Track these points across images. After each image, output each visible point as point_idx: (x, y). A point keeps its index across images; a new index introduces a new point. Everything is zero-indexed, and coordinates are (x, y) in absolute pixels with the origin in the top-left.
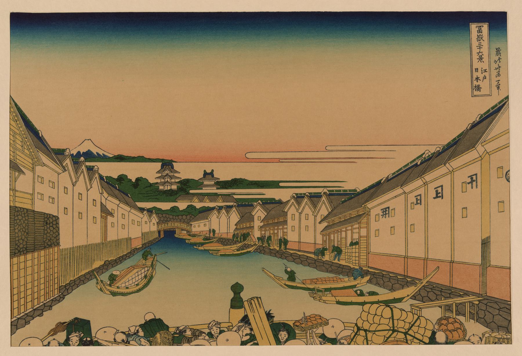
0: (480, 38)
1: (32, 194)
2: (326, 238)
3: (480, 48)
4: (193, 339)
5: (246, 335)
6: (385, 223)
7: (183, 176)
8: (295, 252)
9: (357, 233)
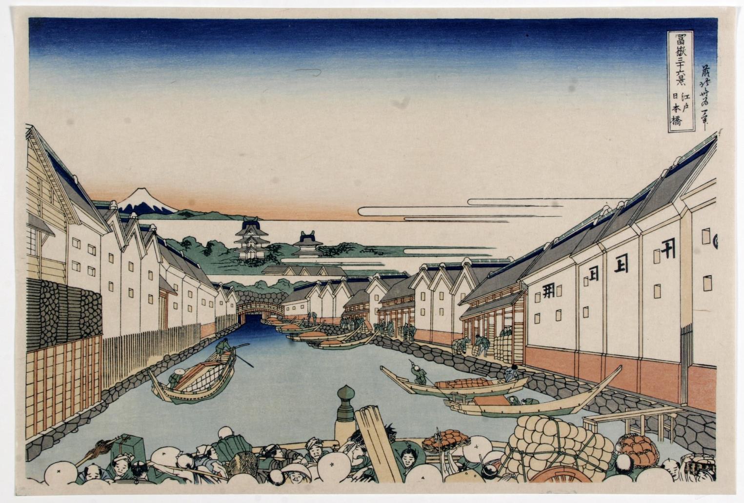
3: (680, 65)
6: (547, 306)
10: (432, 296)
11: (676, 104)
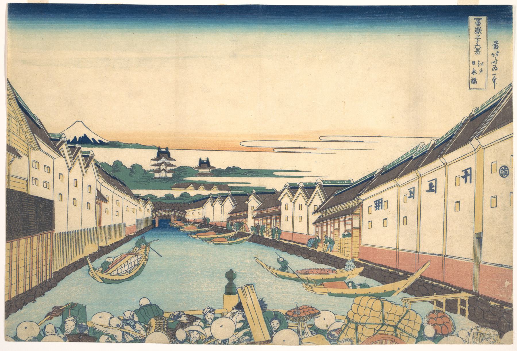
1: (27, 180)
2: (319, 230)
3: (478, 41)
4: (188, 325)
5: (240, 322)
6: (378, 215)
7: (178, 163)
8: (288, 242)
10: (294, 206)
11: (474, 69)
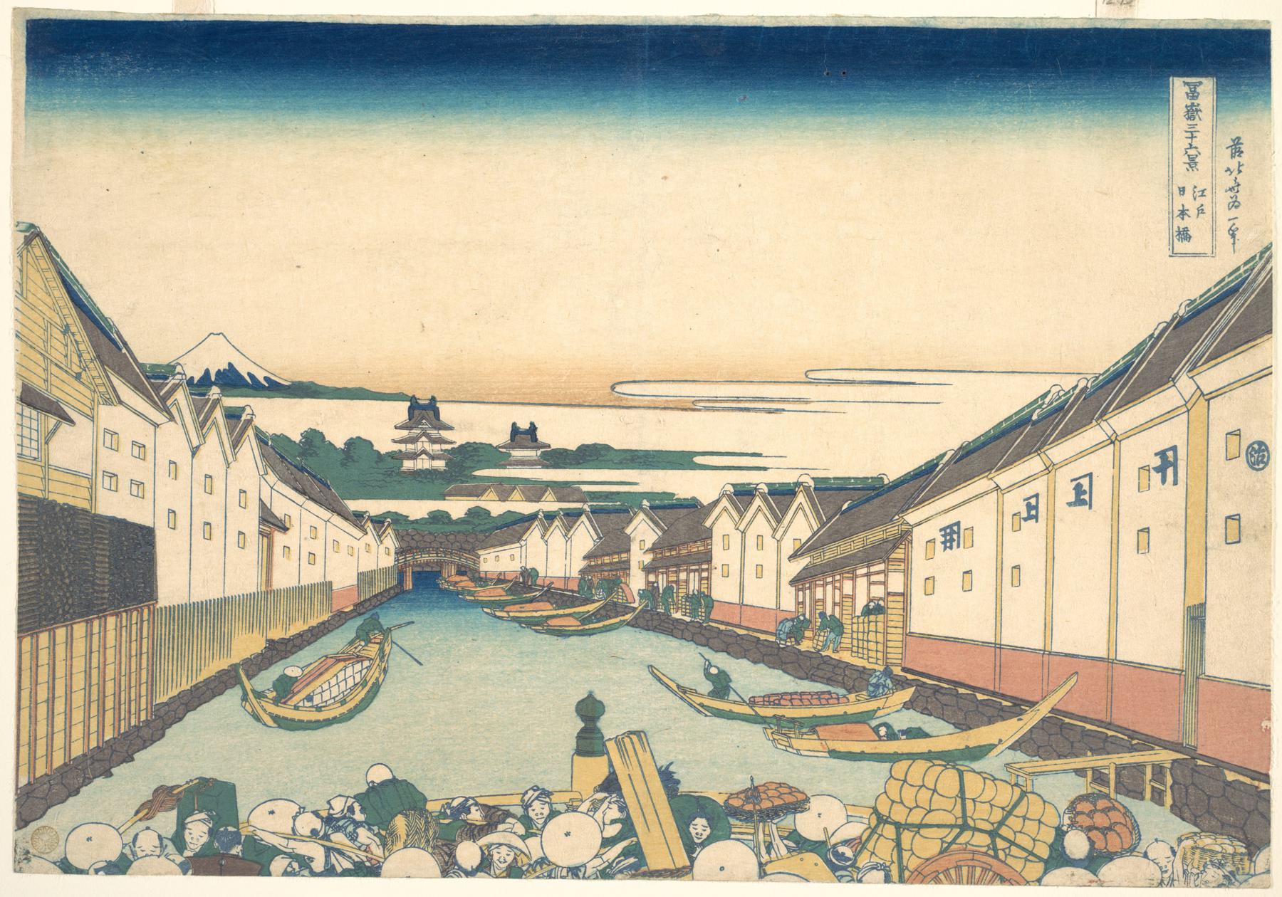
0: (1192, 112)
1: (91, 479)
5: (613, 822)
6: (948, 564)
9: (863, 576)
